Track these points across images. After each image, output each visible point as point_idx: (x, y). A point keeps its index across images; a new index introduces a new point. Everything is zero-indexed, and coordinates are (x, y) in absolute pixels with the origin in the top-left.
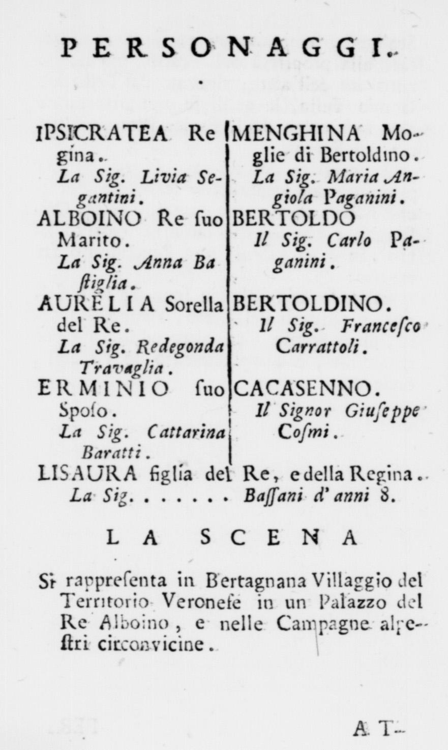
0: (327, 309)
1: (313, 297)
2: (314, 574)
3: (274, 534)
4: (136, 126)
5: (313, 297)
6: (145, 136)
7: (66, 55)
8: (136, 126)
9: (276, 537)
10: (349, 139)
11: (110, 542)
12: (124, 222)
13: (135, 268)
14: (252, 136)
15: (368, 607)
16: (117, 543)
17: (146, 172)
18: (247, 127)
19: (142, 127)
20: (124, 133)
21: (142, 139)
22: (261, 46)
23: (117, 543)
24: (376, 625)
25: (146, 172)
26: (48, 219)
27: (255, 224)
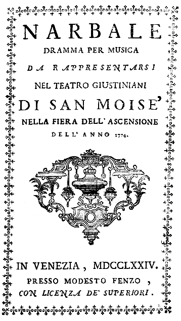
0: (70, 268)
1: (77, 87)
2: (108, 108)
3: (156, 121)
4: (75, 83)
5: (77, 87)
6: (62, 87)
7: (89, 52)
8: (75, 83)
10: (74, 269)
12: (147, 120)
14: (102, 267)
15: (64, 269)
17: (44, 291)
18: (100, 263)
20: (70, 86)
21: (61, 88)
22: (96, 135)
23: (50, 88)
24: (31, 266)
26: (111, 122)
27: (46, 269)
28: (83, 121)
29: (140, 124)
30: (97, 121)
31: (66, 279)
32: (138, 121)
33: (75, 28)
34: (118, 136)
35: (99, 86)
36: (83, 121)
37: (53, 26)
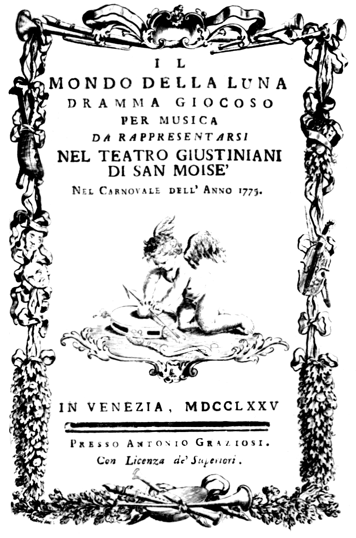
9: (135, 121)
11: (237, 409)
13: (192, 463)
16: (100, 151)
17: (129, 457)
19: (113, 152)
25: (129, 457)
26: (259, 156)
28: (145, 82)
29: (185, 175)
30: (188, 190)
31: (162, 118)
32: (206, 171)
33: (86, 101)
34: (243, 191)
35: (188, 157)
36: (145, 82)
37: (103, 100)
